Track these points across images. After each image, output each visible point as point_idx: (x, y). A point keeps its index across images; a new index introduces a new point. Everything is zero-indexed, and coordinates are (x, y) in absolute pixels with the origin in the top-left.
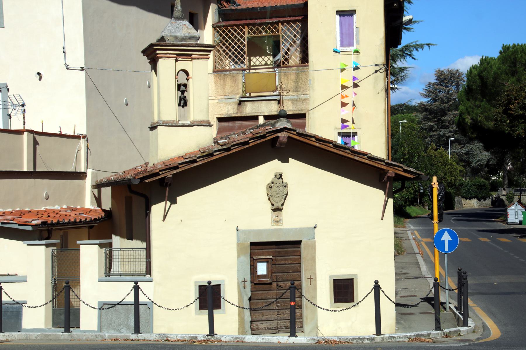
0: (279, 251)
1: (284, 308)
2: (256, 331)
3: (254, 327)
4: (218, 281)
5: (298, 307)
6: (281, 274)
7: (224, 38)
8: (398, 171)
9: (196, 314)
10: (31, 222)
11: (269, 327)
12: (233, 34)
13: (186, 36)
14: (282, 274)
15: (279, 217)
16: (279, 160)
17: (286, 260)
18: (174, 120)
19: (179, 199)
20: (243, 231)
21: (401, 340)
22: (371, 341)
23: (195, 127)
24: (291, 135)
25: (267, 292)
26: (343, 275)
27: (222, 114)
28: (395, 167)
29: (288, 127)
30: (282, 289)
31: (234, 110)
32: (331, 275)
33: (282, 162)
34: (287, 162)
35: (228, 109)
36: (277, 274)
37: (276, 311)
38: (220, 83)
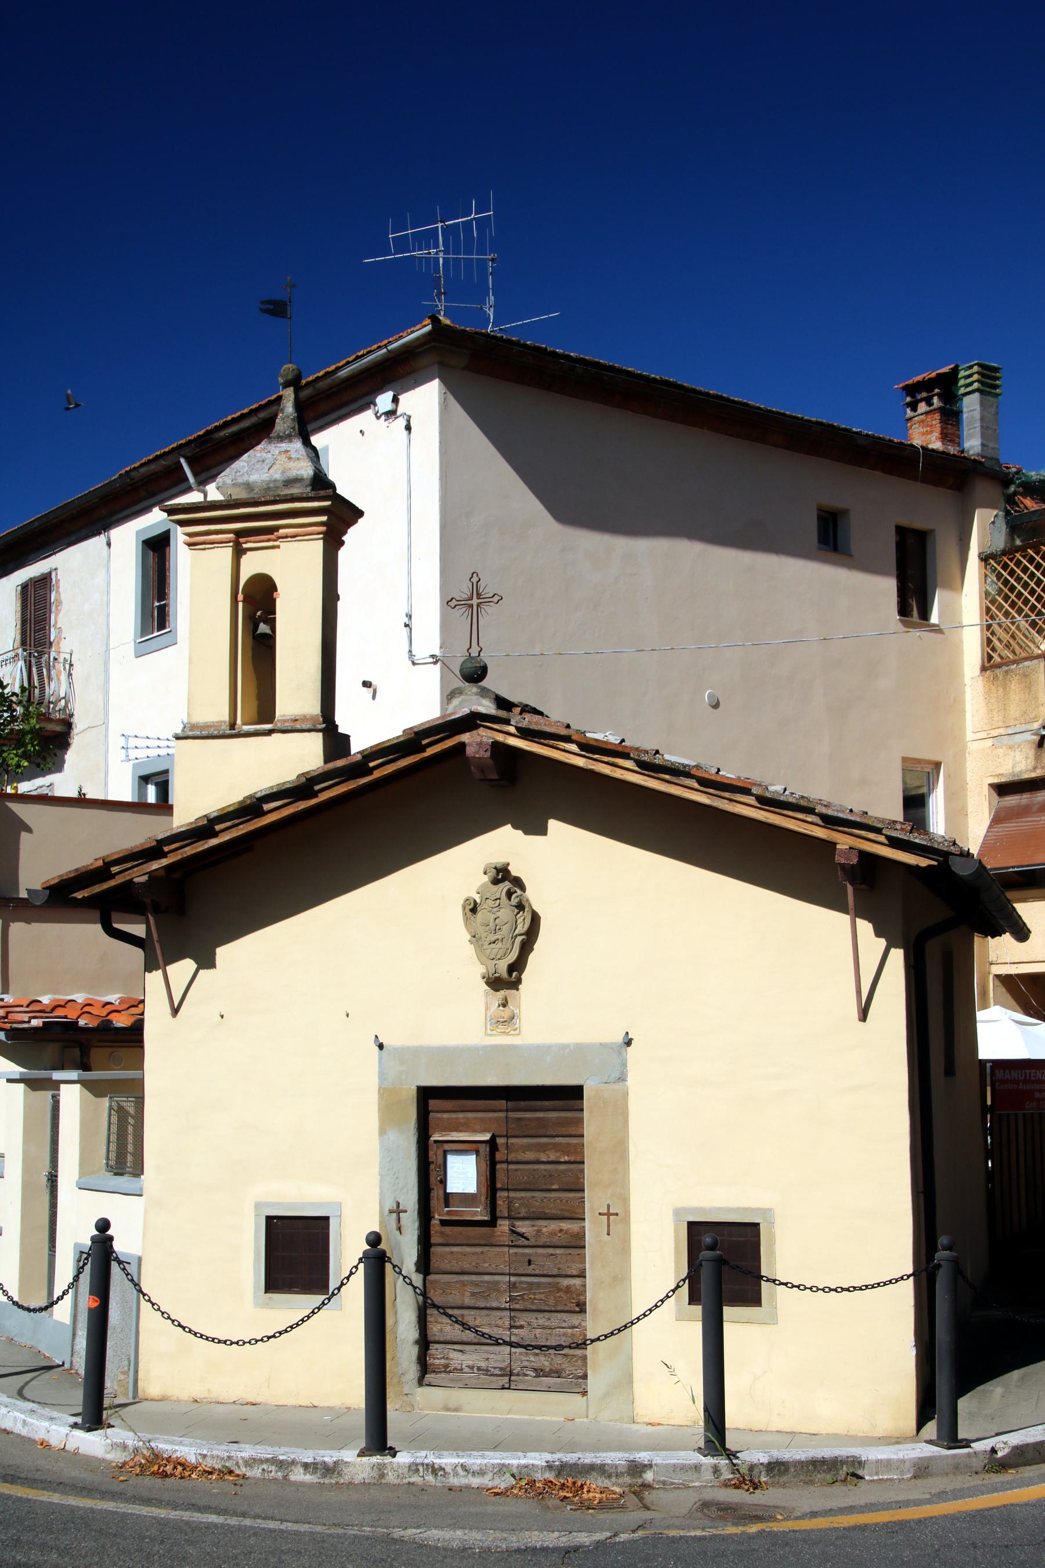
0: (520, 1119)
1: (534, 1307)
2: (443, 1375)
3: (437, 1362)
4: (321, 1205)
5: (577, 1309)
6: (523, 1194)
7: (1006, 582)
8: (868, 843)
9: (257, 1304)
10: (29, 1022)
11: (483, 1364)
12: (1025, 570)
13: (275, 481)
14: (528, 1194)
15: (510, 1005)
16: (515, 827)
17: (542, 1148)
18: (223, 719)
19: (223, 953)
20: (396, 1049)
21: (475, 1482)
22: (324, 1476)
23: (275, 736)
24: (500, 738)
25: (479, 1250)
26: (720, 1209)
27: (1002, 775)
28: (863, 833)
29: (482, 710)
30: (526, 1242)
31: (1029, 761)
32: (680, 1205)
33: (526, 832)
34: (542, 831)
35: (1014, 760)
36: (512, 1194)
37: (507, 1313)
38: (995, 695)
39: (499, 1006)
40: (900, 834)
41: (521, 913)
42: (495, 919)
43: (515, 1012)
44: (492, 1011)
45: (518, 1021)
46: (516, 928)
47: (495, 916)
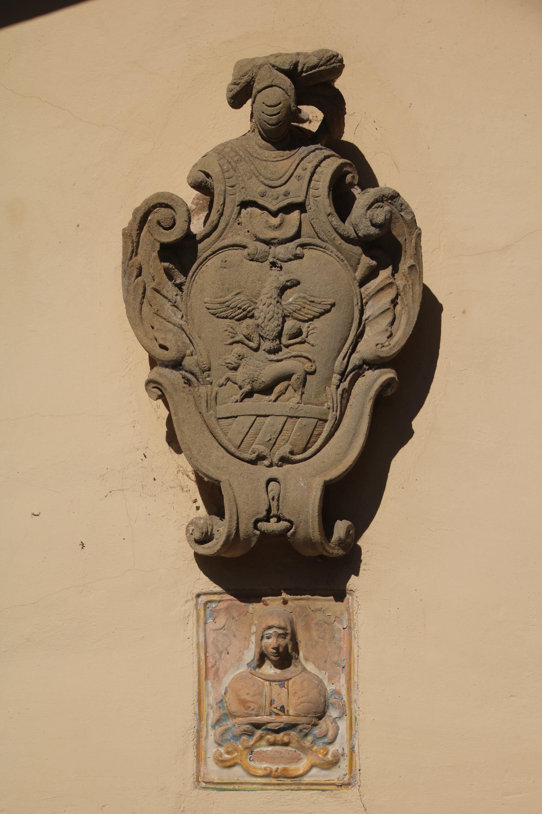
39: (262, 658)
40: (203, 672)
41: (384, 274)
42: (283, 290)
43: (330, 688)
44: (227, 680)
45: (343, 725)
46: (360, 336)
47: (281, 277)
